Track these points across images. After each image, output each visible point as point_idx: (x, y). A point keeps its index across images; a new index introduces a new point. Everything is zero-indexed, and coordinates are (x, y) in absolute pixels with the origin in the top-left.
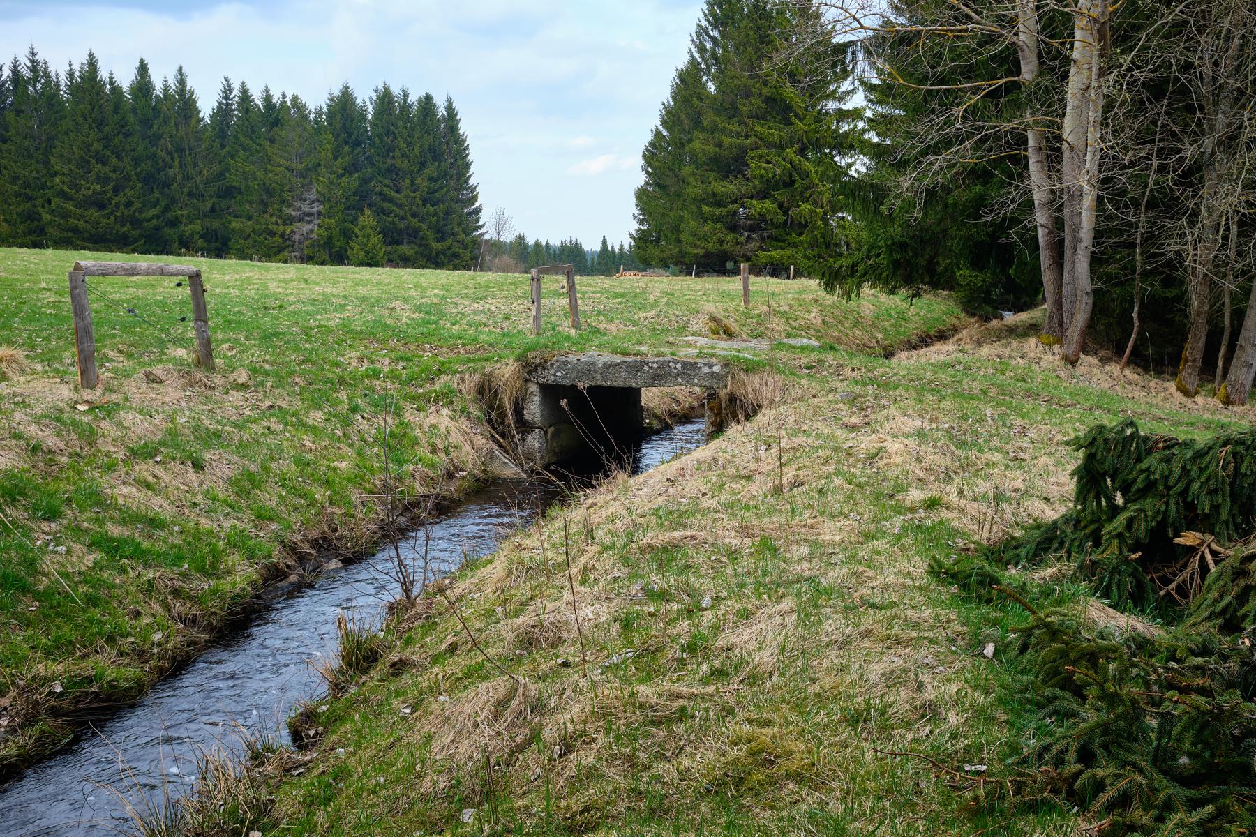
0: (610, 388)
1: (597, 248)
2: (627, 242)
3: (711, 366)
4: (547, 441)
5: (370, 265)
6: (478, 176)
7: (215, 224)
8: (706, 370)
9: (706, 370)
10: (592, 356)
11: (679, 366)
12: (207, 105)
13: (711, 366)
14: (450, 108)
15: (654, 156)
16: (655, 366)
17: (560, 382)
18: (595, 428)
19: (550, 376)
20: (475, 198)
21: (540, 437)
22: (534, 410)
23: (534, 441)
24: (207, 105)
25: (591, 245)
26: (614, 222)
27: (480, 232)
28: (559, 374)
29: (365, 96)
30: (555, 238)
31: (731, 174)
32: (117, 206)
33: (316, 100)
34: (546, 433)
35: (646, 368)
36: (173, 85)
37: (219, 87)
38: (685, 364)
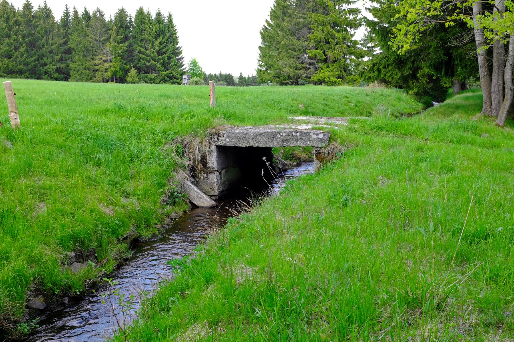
0: (257, 147)
1: (238, 75)
2: (255, 73)
3: (317, 134)
4: (221, 177)
5: (134, 83)
6: (182, 43)
7: (63, 65)
8: (314, 136)
9: (314, 136)
10: (246, 130)
11: (298, 134)
12: (58, 16)
13: (317, 134)
14: (170, 16)
15: (266, 35)
16: (284, 134)
17: (229, 144)
18: (249, 173)
19: (224, 141)
20: (180, 53)
21: (217, 176)
22: (213, 161)
23: (214, 178)
24: (58, 16)
25: (236, 75)
26: (246, 62)
27: (183, 68)
28: (227, 140)
29: (132, 13)
30: (216, 72)
31: (302, 42)
32: (17, 57)
33: (110, 14)
34: (220, 173)
35: (279, 136)
36: (110, 20)
37: (63, 9)
38: (302, 133)
